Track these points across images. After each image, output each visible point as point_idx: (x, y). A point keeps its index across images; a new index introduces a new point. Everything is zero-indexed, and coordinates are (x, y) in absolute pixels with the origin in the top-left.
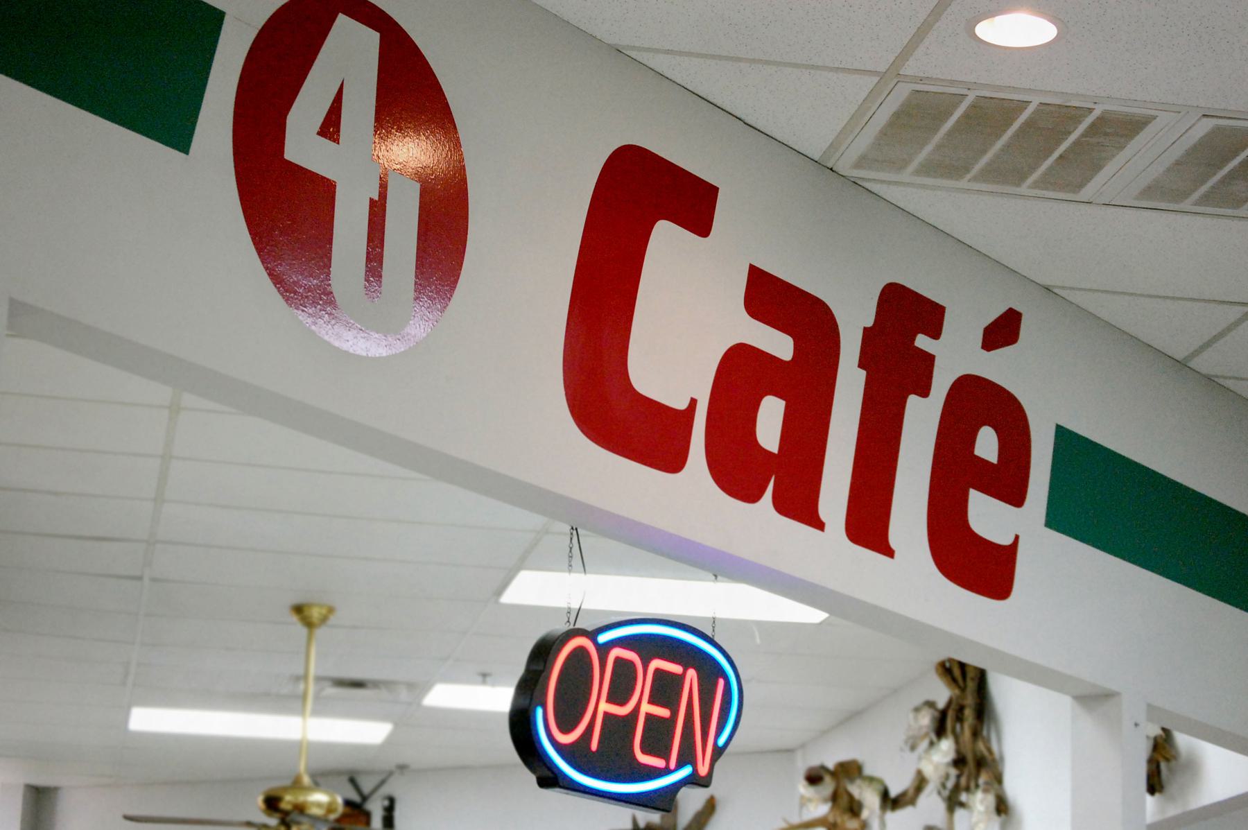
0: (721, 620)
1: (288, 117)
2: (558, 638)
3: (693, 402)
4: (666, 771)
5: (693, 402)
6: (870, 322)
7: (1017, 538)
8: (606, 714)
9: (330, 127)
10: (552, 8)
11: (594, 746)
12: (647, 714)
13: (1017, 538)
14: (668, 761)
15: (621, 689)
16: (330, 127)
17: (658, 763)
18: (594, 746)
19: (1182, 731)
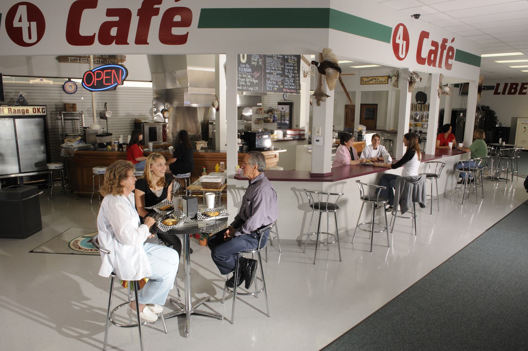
0: (311, 88)
1: (13, 22)
2: (200, 155)
3: (95, 34)
4: (112, 85)
5: (95, 34)
6: (140, 7)
7: (188, 33)
8: (97, 81)
9: (20, 20)
10: (92, 348)
11: (95, 85)
12: (105, 78)
13: (188, 33)
14: (111, 83)
15: (99, 75)
16: (20, 20)
17: (110, 84)
18: (95, 85)
19: (304, 54)
